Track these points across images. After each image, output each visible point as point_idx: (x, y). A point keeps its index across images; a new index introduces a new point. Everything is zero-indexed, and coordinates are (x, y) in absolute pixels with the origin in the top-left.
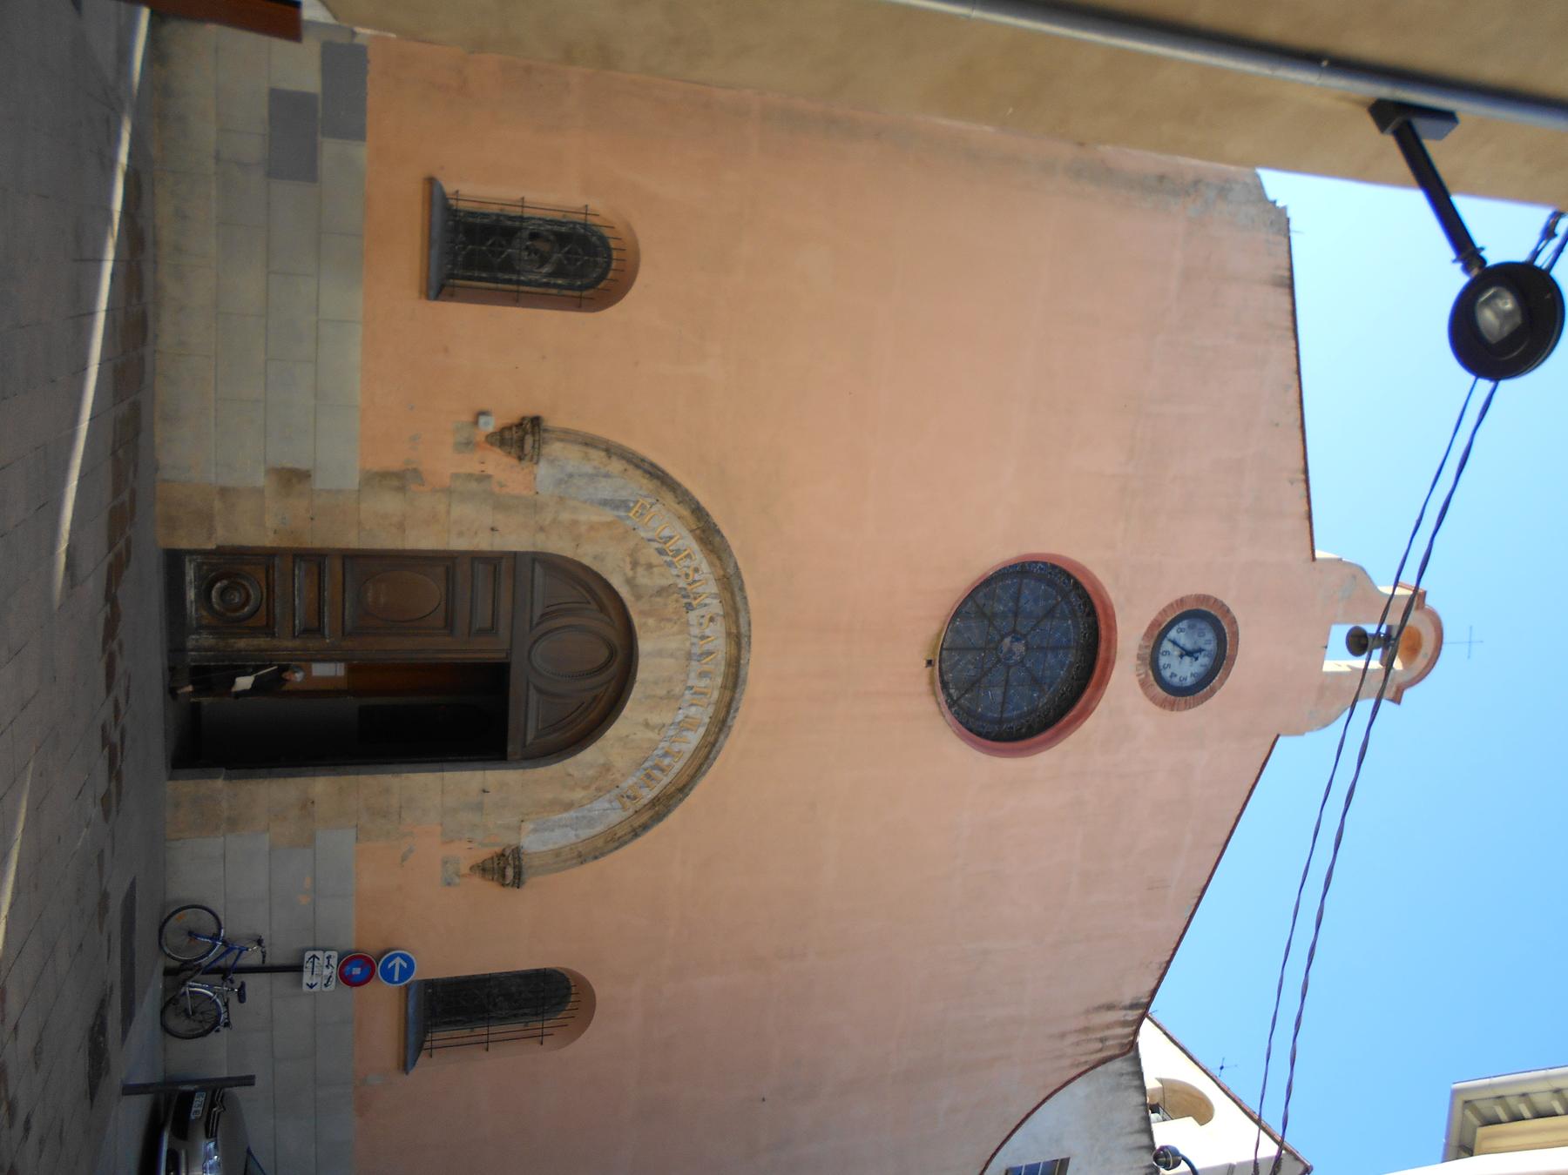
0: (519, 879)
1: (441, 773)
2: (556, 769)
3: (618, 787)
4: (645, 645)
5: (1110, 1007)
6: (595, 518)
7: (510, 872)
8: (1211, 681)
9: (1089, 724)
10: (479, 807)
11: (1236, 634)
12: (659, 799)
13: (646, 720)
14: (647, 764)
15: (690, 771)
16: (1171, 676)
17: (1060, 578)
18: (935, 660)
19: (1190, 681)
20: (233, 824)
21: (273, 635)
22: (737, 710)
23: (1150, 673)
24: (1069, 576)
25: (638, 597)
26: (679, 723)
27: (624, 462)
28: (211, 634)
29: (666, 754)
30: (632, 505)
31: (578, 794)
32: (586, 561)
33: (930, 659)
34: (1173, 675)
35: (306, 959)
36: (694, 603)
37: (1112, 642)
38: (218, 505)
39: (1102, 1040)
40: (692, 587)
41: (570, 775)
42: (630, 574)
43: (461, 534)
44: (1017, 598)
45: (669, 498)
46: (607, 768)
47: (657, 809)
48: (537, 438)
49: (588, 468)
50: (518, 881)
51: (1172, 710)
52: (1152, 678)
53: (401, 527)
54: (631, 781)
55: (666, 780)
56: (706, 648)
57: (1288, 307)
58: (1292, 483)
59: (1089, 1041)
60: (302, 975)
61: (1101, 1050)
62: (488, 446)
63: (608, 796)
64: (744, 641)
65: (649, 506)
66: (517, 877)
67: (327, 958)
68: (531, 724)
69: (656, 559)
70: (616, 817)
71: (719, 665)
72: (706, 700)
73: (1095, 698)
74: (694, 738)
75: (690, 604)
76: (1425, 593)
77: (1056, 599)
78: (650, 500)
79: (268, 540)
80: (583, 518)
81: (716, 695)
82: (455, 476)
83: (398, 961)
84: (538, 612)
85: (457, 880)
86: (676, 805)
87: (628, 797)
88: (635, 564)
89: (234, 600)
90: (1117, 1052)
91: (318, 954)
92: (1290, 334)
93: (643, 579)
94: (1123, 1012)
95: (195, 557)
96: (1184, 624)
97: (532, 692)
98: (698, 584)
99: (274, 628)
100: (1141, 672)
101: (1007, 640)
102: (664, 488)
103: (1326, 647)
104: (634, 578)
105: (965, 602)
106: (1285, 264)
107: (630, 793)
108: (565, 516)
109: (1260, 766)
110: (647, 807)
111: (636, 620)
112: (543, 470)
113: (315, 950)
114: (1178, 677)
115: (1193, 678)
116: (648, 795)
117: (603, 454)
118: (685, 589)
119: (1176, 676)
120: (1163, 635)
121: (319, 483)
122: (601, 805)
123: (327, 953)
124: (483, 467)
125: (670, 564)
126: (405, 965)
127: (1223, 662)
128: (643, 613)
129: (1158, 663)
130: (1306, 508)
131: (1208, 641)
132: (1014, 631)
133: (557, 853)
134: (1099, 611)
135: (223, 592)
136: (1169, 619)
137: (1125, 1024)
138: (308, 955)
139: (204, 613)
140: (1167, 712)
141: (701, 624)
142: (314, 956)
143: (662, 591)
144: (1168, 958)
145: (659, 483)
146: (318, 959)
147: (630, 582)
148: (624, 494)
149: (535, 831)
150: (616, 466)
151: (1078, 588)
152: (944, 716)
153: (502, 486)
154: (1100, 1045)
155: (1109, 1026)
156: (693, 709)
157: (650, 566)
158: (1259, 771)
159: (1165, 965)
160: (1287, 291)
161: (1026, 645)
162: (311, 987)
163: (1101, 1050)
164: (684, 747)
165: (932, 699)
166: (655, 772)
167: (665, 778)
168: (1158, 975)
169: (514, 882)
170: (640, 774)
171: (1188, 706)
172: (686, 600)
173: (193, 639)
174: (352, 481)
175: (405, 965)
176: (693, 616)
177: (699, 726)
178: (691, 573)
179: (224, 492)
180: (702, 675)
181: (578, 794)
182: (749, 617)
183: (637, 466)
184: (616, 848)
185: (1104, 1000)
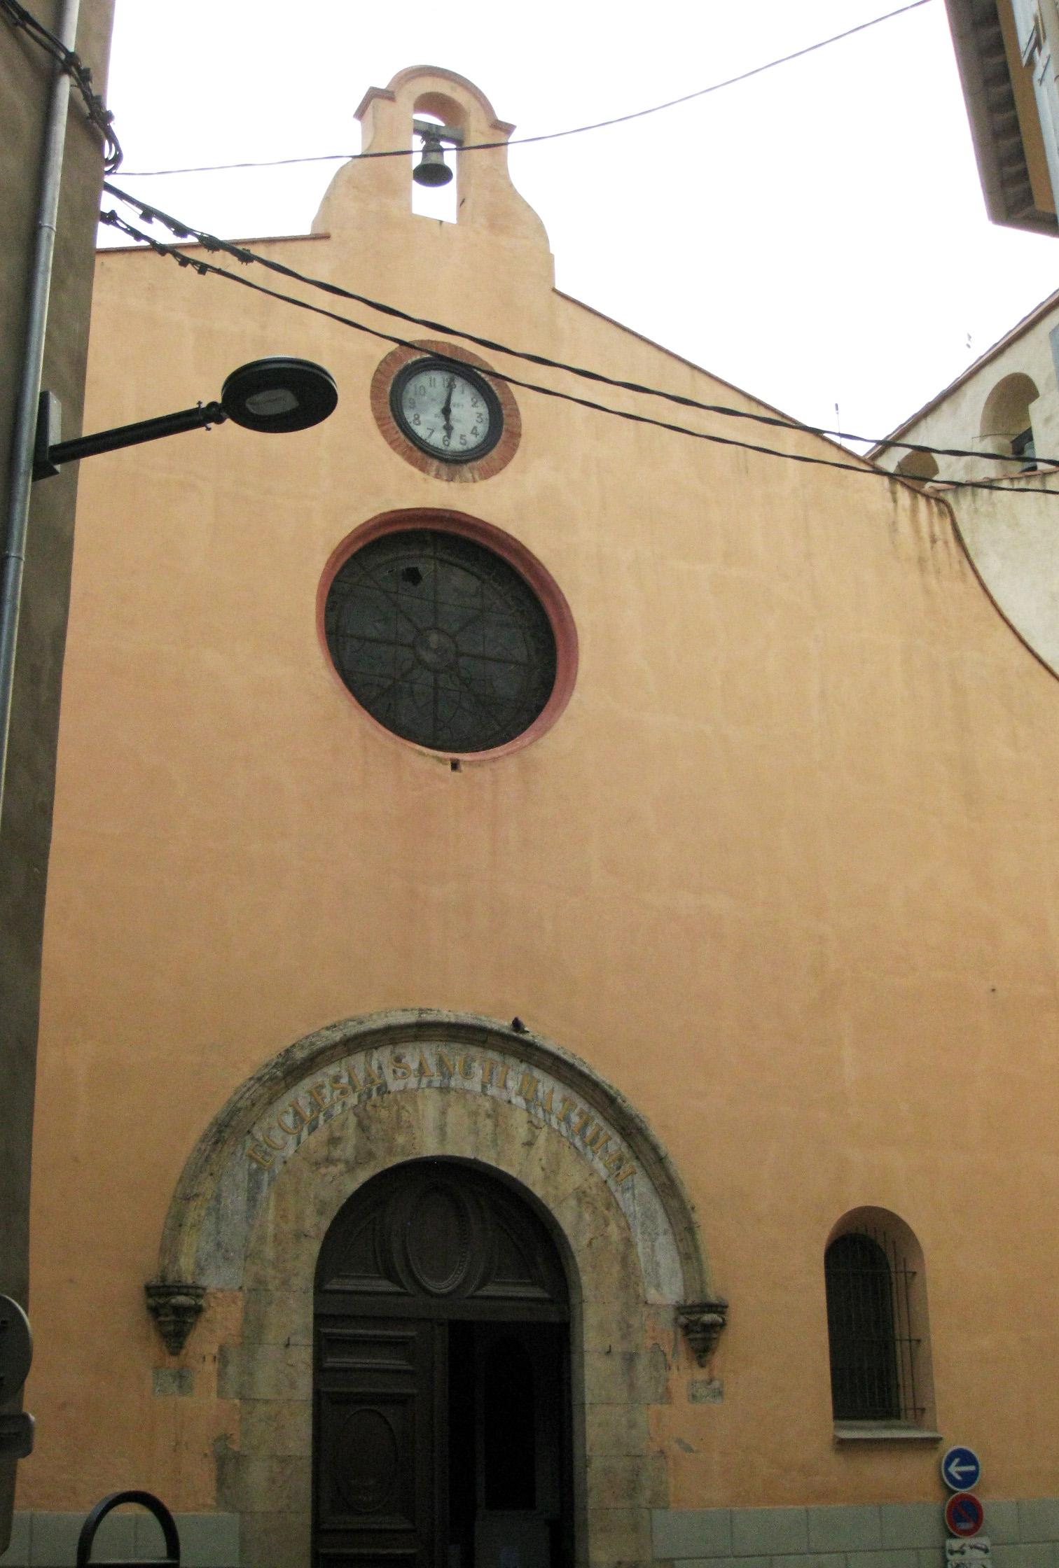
4: (430, 1147)
7: (708, 1318)
16: (476, 435)
19: (482, 409)
29: (566, 1119)
32: (326, 1224)
34: (474, 431)
42: (341, 1167)
43: (293, 1385)
46: (581, 1196)
49: (209, 1225)
50: (720, 1308)
53: (284, 1461)
54: (599, 1165)
69: (322, 1133)
71: (456, 1054)
80: (271, 1229)
82: (221, 1393)
83: (953, 1469)
85: (716, 1384)
88: (329, 1161)
94: (900, 510)
96: (409, 415)
104: (347, 1162)
108: (269, 1252)
112: (211, 1281)
115: (478, 404)
119: (475, 428)
122: (624, 1199)
124: (209, 1358)
125: (329, 1116)
126: (957, 1460)
131: (433, 384)
140: (522, 441)
141: (404, 1074)
147: (351, 1168)
154: (940, 543)
157: (334, 1141)
163: (946, 543)
176: (394, 1085)
181: (613, 1231)
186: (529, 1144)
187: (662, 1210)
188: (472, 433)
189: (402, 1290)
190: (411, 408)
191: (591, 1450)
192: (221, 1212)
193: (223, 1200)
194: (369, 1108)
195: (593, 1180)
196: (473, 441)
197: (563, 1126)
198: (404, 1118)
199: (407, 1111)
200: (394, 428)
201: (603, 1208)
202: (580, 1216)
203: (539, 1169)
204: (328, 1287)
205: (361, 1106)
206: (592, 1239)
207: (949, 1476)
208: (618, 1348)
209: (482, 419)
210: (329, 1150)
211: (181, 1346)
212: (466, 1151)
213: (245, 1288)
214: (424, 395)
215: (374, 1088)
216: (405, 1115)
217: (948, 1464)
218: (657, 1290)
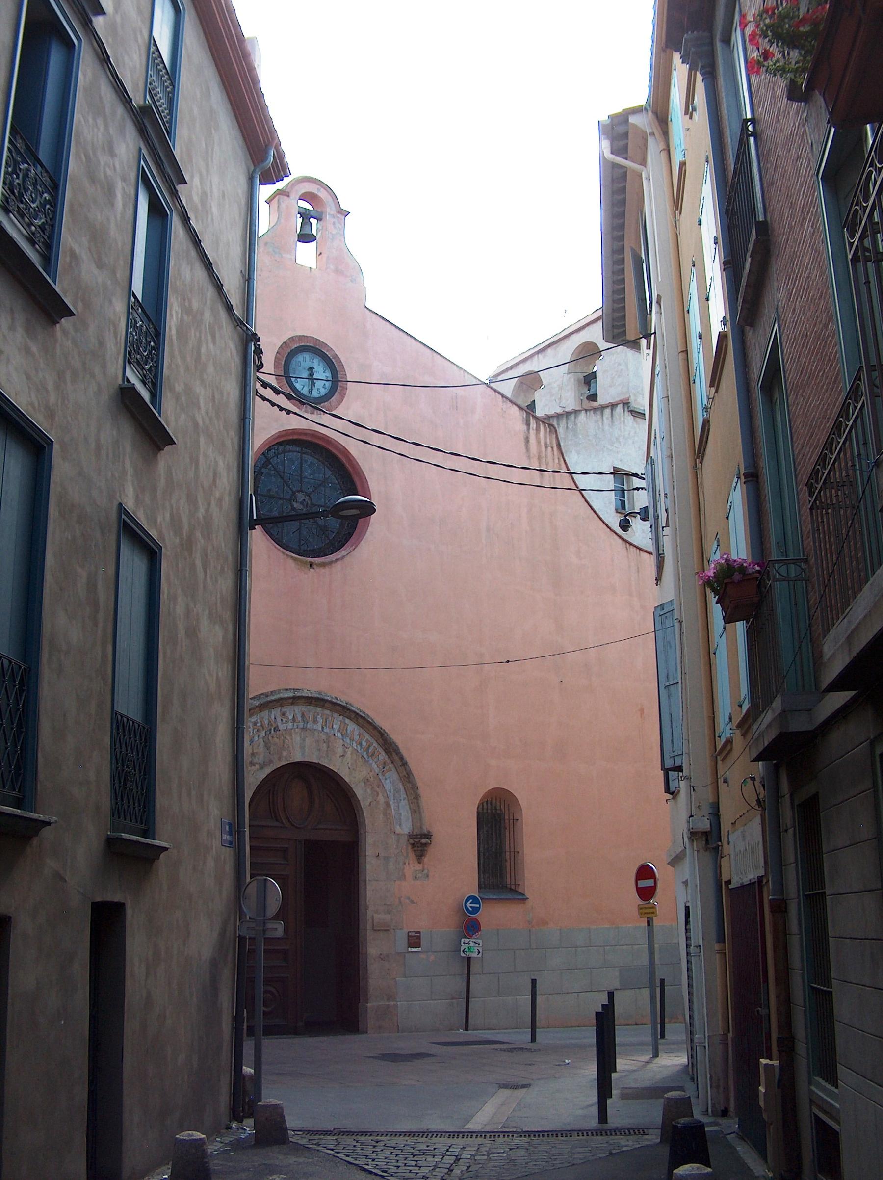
4: (298, 758)
5: (527, 440)
7: (424, 841)
13: (340, 756)
14: (365, 756)
25: (271, 762)
29: (360, 744)
31: (381, 799)
39: (546, 448)
42: (257, 767)
46: (366, 781)
54: (375, 766)
56: (300, 719)
61: (552, 448)
70: (394, 776)
74: (351, 726)
83: (468, 905)
85: (425, 872)
87: (384, 768)
94: (531, 430)
104: (260, 764)
107: (381, 767)
110: (390, 756)
116: (383, 756)
118: (266, 732)
122: (388, 786)
123: (462, 944)
126: (471, 901)
128: (279, 759)
131: (305, 361)
137: (538, 430)
141: (286, 721)
142: (463, 951)
143: (267, 746)
149: (400, 825)
155: (539, 442)
156: (335, 726)
159: (504, 399)
161: (298, 491)
162: (479, 952)
163: (552, 448)
164: (356, 732)
167: (374, 745)
175: (471, 901)
180: (315, 721)
181: (381, 799)
191: (369, 901)
194: (270, 738)
207: (466, 906)
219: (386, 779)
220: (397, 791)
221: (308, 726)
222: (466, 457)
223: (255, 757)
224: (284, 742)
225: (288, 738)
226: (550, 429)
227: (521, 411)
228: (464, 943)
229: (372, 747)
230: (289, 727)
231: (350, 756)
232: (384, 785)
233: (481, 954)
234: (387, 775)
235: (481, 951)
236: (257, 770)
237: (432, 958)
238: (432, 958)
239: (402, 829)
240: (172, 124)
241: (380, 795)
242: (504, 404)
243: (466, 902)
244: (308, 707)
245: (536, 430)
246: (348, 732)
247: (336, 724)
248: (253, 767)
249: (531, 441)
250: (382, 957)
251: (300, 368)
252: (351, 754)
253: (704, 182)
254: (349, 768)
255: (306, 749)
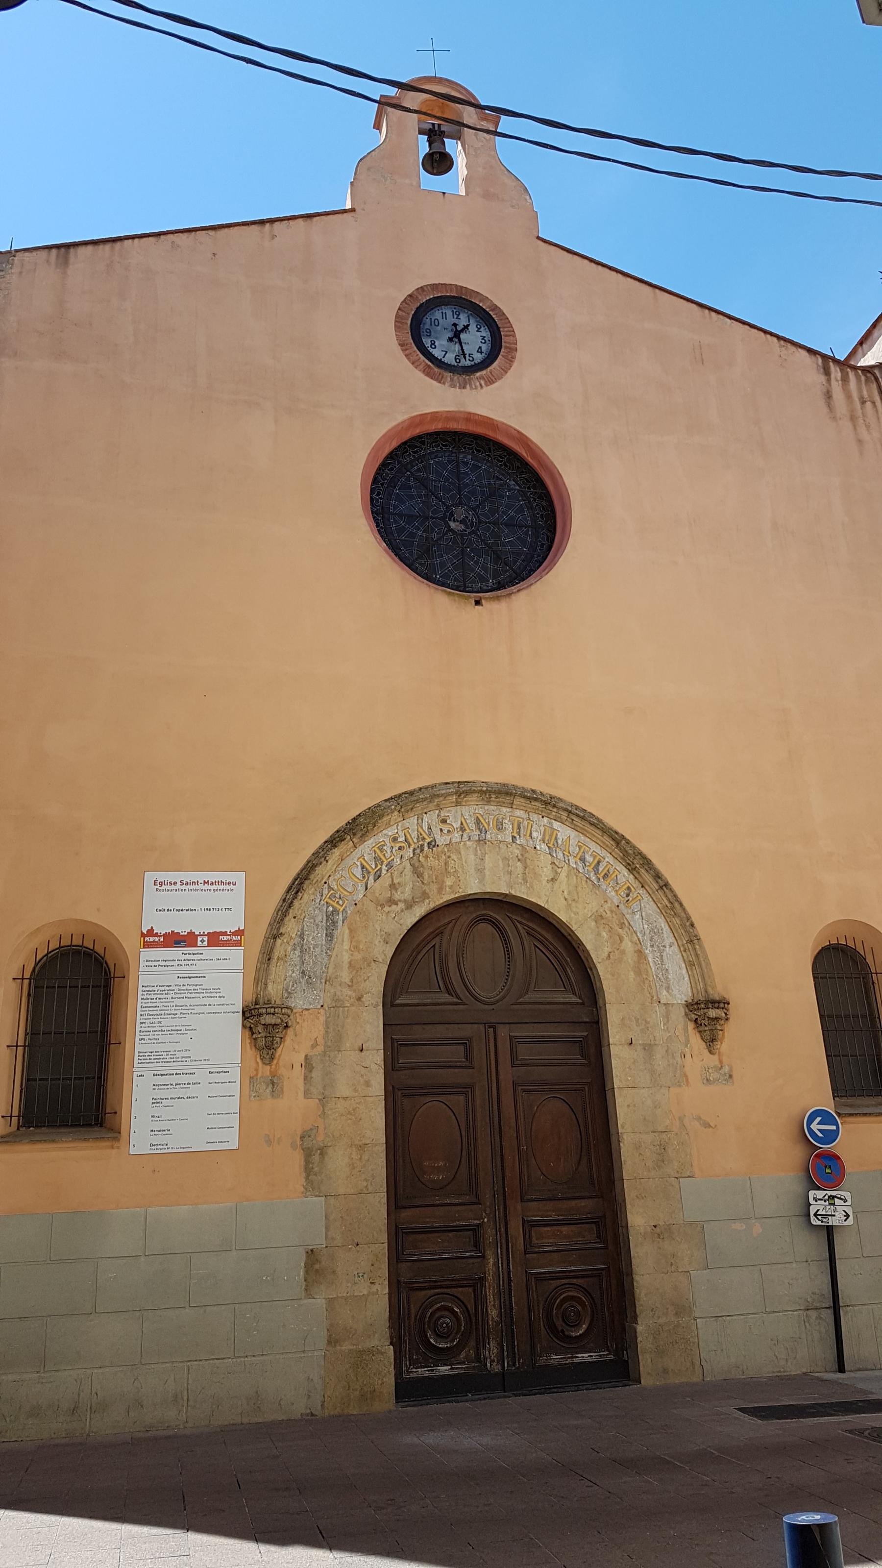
0: (719, 1002)
1: (616, 1090)
2: (602, 969)
3: (618, 906)
4: (473, 887)
5: (828, 395)
6: (346, 946)
7: (712, 1013)
8: (484, 310)
9: (533, 436)
10: (648, 1048)
11: (434, 287)
12: (629, 864)
13: (548, 881)
14: (593, 878)
15: (598, 833)
16: (481, 353)
17: (387, 475)
18: (475, 597)
19: (485, 333)
20: (682, 1309)
21: (482, 1279)
22: (533, 791)
23: (478, 374)
24: (384, 465)
25: (425, 895)
26: (549, 848)
27: (287, 919)
28: (484, 1347)
29: (583, 860)
30: (331, 909)
31: (628, 945)
32: (390, 951)
33: (474, 603)
34: (480, 350)
35: (819, 1223)
36: (428, 840)
37: (450, 416)
38: (346, 1347)
39: (863, 402)
40: (411, 843)
41: (609, 956)
42: (401, 905)
43: (368, 1084)
44: (410, 518)
45: (322, 871)
46: (599, 918)
47: (638, 866)
48: (264, 1011)
49: (295, 956)
50: (722, 1004)
51: (516, 350)
52: (484, 372)
53: (361, 1148)
54: (611, 893)
55: (609, 858)
56: (473, 826)
57: (90, 248)
58: (274, 237)
59: (864, 415)
60: (835, 1226)
61: (874, 403)
62: (275, 1061)
63: (628, 916)
64: (464, 788)
65: (332, 892)
66: (717, 1005)
67: (816, 1201)
68: (561, 998)
69: (385, 880)
70: (650, 907)
71: (491, 812)
72: (526, 823)
73: (507, 430)
74: (564, 832)
75: (429, 843)
76: (381, 96)
77: (409, 477)
78: (325, 892)
79: (382, 1289)
80: (346, 957)
81: (519, 813)
82: (307, 1094)
83: (815, 1126)
84: (446, 998)
85: (726, 1069)
86: (634, 847)
87: (628, 895)
88: (392, 902)
89: (447, 1324)
90: (875, 386)
91: (813, 1210)
92: (118, 245)
93: (405, 893)
94: (833, 382)
95: (404, 1368)
96: (427, 342)
97: (526, 998)
98: (408, 836)
99: (475, 1279)
100: (478, 384)
101: (453, 525)
102: (312, 877)
103: (444, 193)
104: (405, 901)
105: (415, 570)
106: (44, 254)
107: (623, 893)
108: (345, 976)
109: (571, 255)
110: (637, 876)
111: (447, 897)
112: (298, 1002)
113: (809, 1215)
114: (481, 345)
115: (482, 329)
116: (624, 875)
117: (279, 941)
118: (414, 850)
119: (480, 348)
120: (439, 363)
121: (319, 1241)
122: (637, 922)
123: (812, 1201)
124: (297, 1066)
125: (390, 866)
126: (819, 1119)
127: (464, 299)
128: (440, 890)
129: (469, 367)
130: (300, 220)
131: (445, 317)
132: (443, 519)
133: (690, 965)
134: (417, 431)
135: (439, 1336)
136: (422, 358)
137: (845, 379)
138: (815, 1222)
139: (463, 1355)
140: (518, 354)
141: (449, 831)
142: (816, 1215)
143: (417, 872)
144: (775, 339)
145: (307, 882)
146: (818, 1210)
147: (409, 905)
148: (320, 917)
149: (668, 989)
150: (291, 927)
151: (396, 455)
152: (531, 585)
153: (315, 1045)
154: (869, 404)
155: (849, 397)
156: (535, 834)
157: (393, 886)
158: (575, 257)
159: (782, 342)
160: (72, 250)
161: (456, 505)
162: (847, 1216)
163: (874, 403)
164: (573, 842)
165: (513, 597)
166: (601, 869)
167: (607, 859)
168: (792, 349)
169: (723, 1008)
170: (603, 884)
171: (512, 333)
172: (426, 848)
173: (491, 1365)
174: (318, 1202)
175: (819, 1119)
176: (441, 840)
177: (552, 828)
178: (398, 845)
179: (332, 1341)
180: (500, 827)
181: (628, 945)
182: (440, 784)
183: (290, 905)
184: (681, 904)
185: (821, 403)
186: (553, 880)
187: (667, 927)
188: (478, 352)
189: (460, 1001)
190: (427, 336)
191: (623, 1127)
192: (304, 947)
193: (306, 938)
194: (421, 859)
195: (606, 906)
196: (478, 358)
197: (580, 864)
198: (451, 865)
199: (453, 860)
200: (505, 342)
201: (617, 928)
202: (599, 934)
203: (562, 899)
204: (398, 1002)
205: (415, 858)
206: (610, 952)
207: (810, 1130)
208: (639, 1041)
209: (485, 340)
210: (391, 893)
211: (272, 1058)
212: (502, 888)
213: (325, 1006)
214: (438, 326)
215: (426, 845)
216: (451, 863)
217: (811, 1120)
218: (668, 992)
219: (634, 913)
220: (656, 932)
221: (488, 836)
222: (224, 1128)
223: (396, 890)
224: (446, 864)
225: (454, 856)
226: (866, 376)
227: (813, 357)
228: (816, 1200)
229: (605, 864)
230: (454, 840)
231: (566, 879)
232: (632, 923)
233: (851, 1218)
234: (635, 906)
235: (850, 1213)
236: (402, 911)
237: (757, 1229)
238: (757, 1229)
239: (671, 995)
240: (838, 1125)
241: (626, 939)
242: (783, 349)
243: (809, 1123)
244: (486, 807)
245: (842, 380)
246: (560, 842)
247: (536, 831)
248: (394, 907)
249: (834, 396)
250: (658, 1230)
251: (439, 328)
252: (567, 876)
253: (167, 1132)
254: (566, 899)
255: (487, 873)
